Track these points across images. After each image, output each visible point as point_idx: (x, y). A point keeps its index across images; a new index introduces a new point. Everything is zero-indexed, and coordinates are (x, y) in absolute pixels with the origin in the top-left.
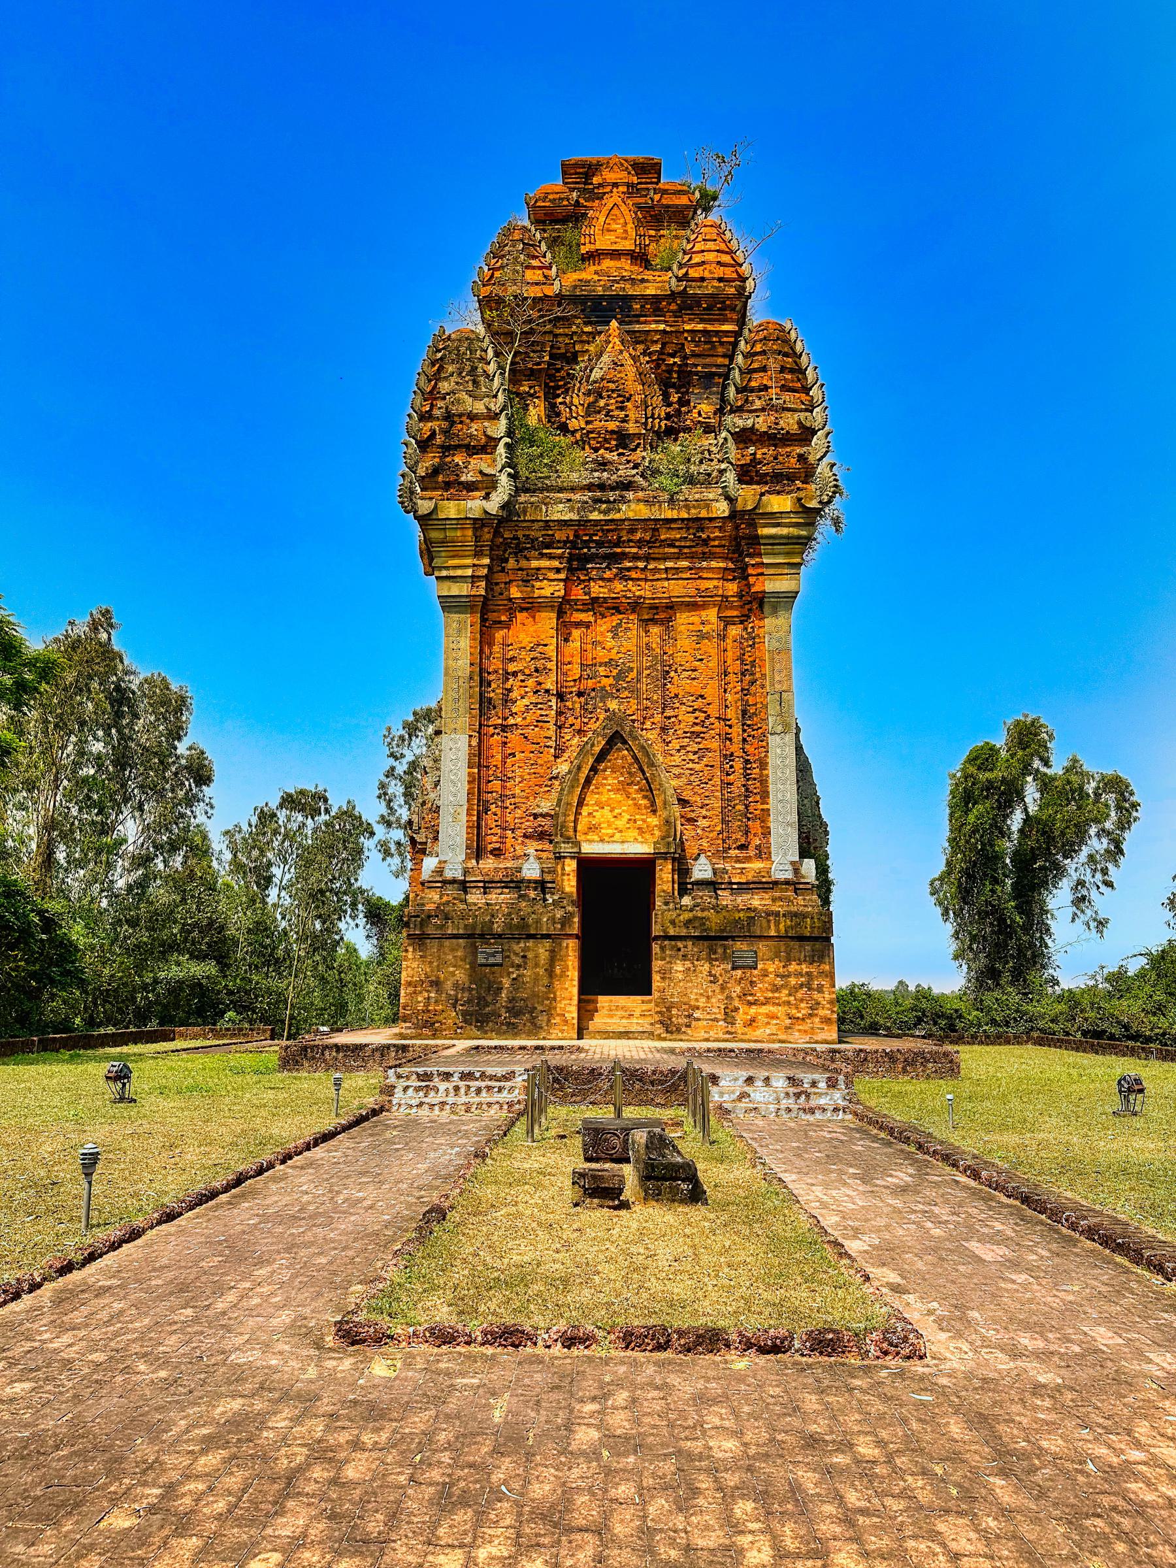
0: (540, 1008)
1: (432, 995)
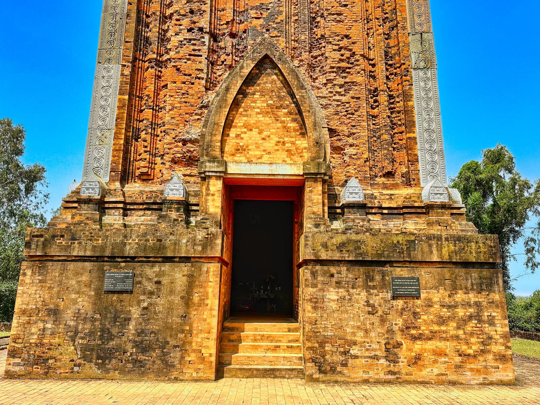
0: (172, 342)
1: (49, 326)
